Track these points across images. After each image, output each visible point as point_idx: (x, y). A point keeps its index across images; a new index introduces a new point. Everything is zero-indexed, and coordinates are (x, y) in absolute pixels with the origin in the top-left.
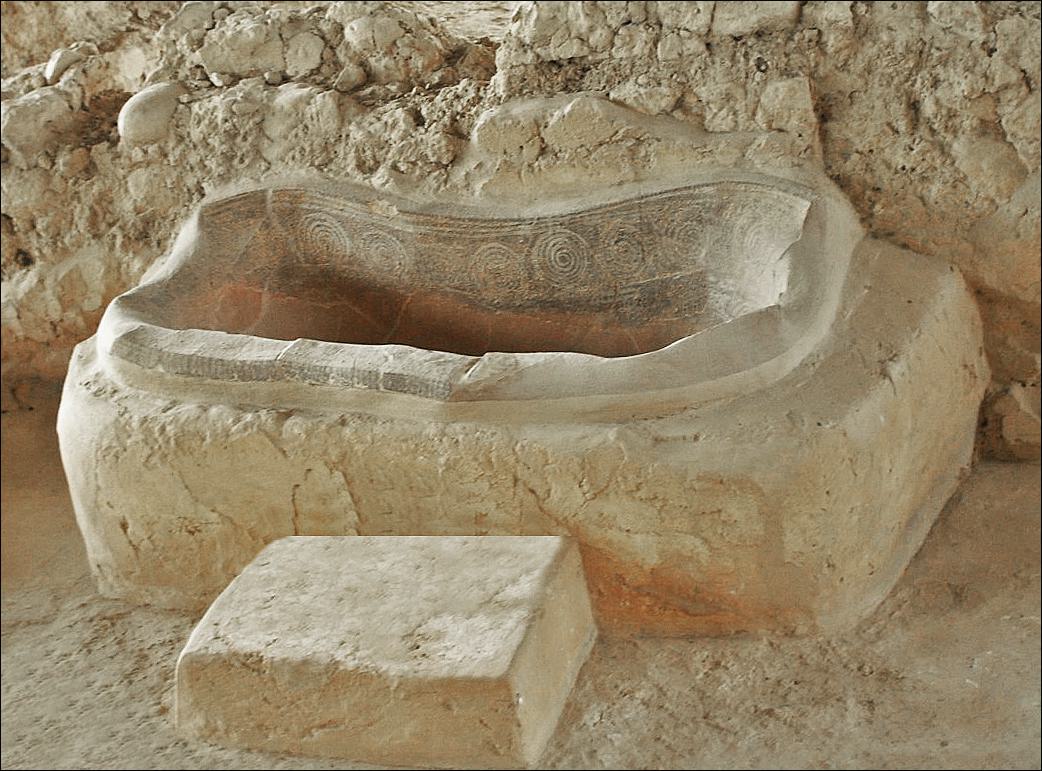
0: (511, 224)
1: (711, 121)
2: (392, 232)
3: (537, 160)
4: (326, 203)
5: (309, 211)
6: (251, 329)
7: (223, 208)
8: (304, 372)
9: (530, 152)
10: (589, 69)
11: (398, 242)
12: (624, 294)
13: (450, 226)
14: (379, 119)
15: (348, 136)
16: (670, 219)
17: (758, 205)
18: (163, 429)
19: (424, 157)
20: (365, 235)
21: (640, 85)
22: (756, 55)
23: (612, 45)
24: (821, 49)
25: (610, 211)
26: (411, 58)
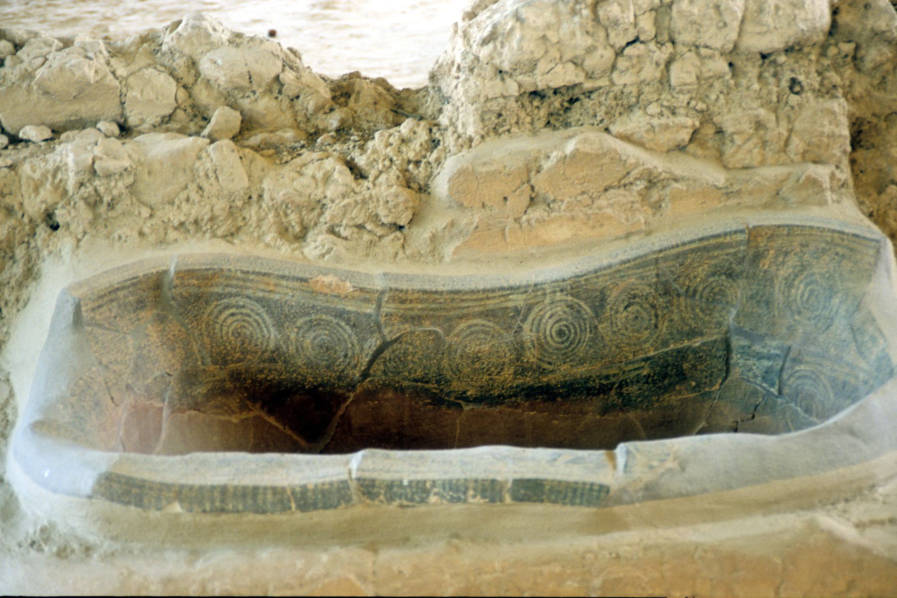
0: (500, 293)
1: (732, 156)
2: (340, 314)
3: (525, 212)
4: (248, 284)
5: (220, 296)
6: (322, 444)
7: (105, 299)
8: (392, 490)
9: (518, 201)
10: (577, 100)
11: (347, 328)
12: (630, 371)
13: (426, 301)
14: (301, 174)
15: (260, 196)
16: (692, 276)
17: (805, 250)
20: (300, 322)
21: (652, 116)
22: (788, 75)
23: (614, 67)
24: (855, 65)
25: (617, 272)
26: (298, 97)
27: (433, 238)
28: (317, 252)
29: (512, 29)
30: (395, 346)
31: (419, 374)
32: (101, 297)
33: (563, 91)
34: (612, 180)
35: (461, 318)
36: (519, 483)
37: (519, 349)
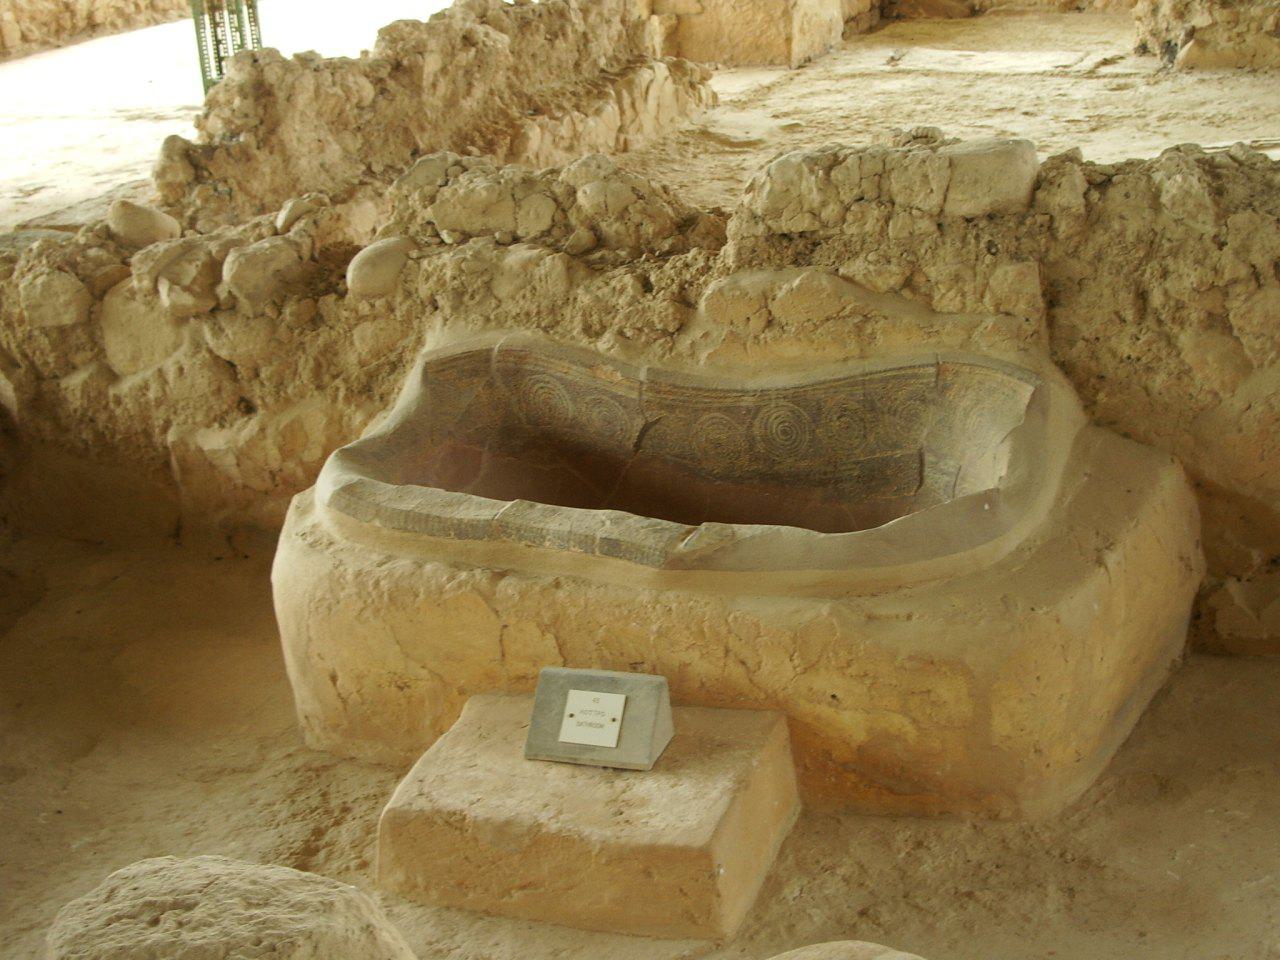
2: (615, 397)
9: (757, 323)
14: (607, 284)
18: (377, 584)
19: (650, 324)
20: (588, 399)
23: (844, 220)
25: (833, 386)
27: (693, 344)
28: (605, 346)
29: (764, 184)
30: (657, 426)
31: (677, 451)
32: (443, 363)
33: (808, 235)
34: (832, 312)
35: (705, 410)
36: (606, 540)
37: (751, 441)
